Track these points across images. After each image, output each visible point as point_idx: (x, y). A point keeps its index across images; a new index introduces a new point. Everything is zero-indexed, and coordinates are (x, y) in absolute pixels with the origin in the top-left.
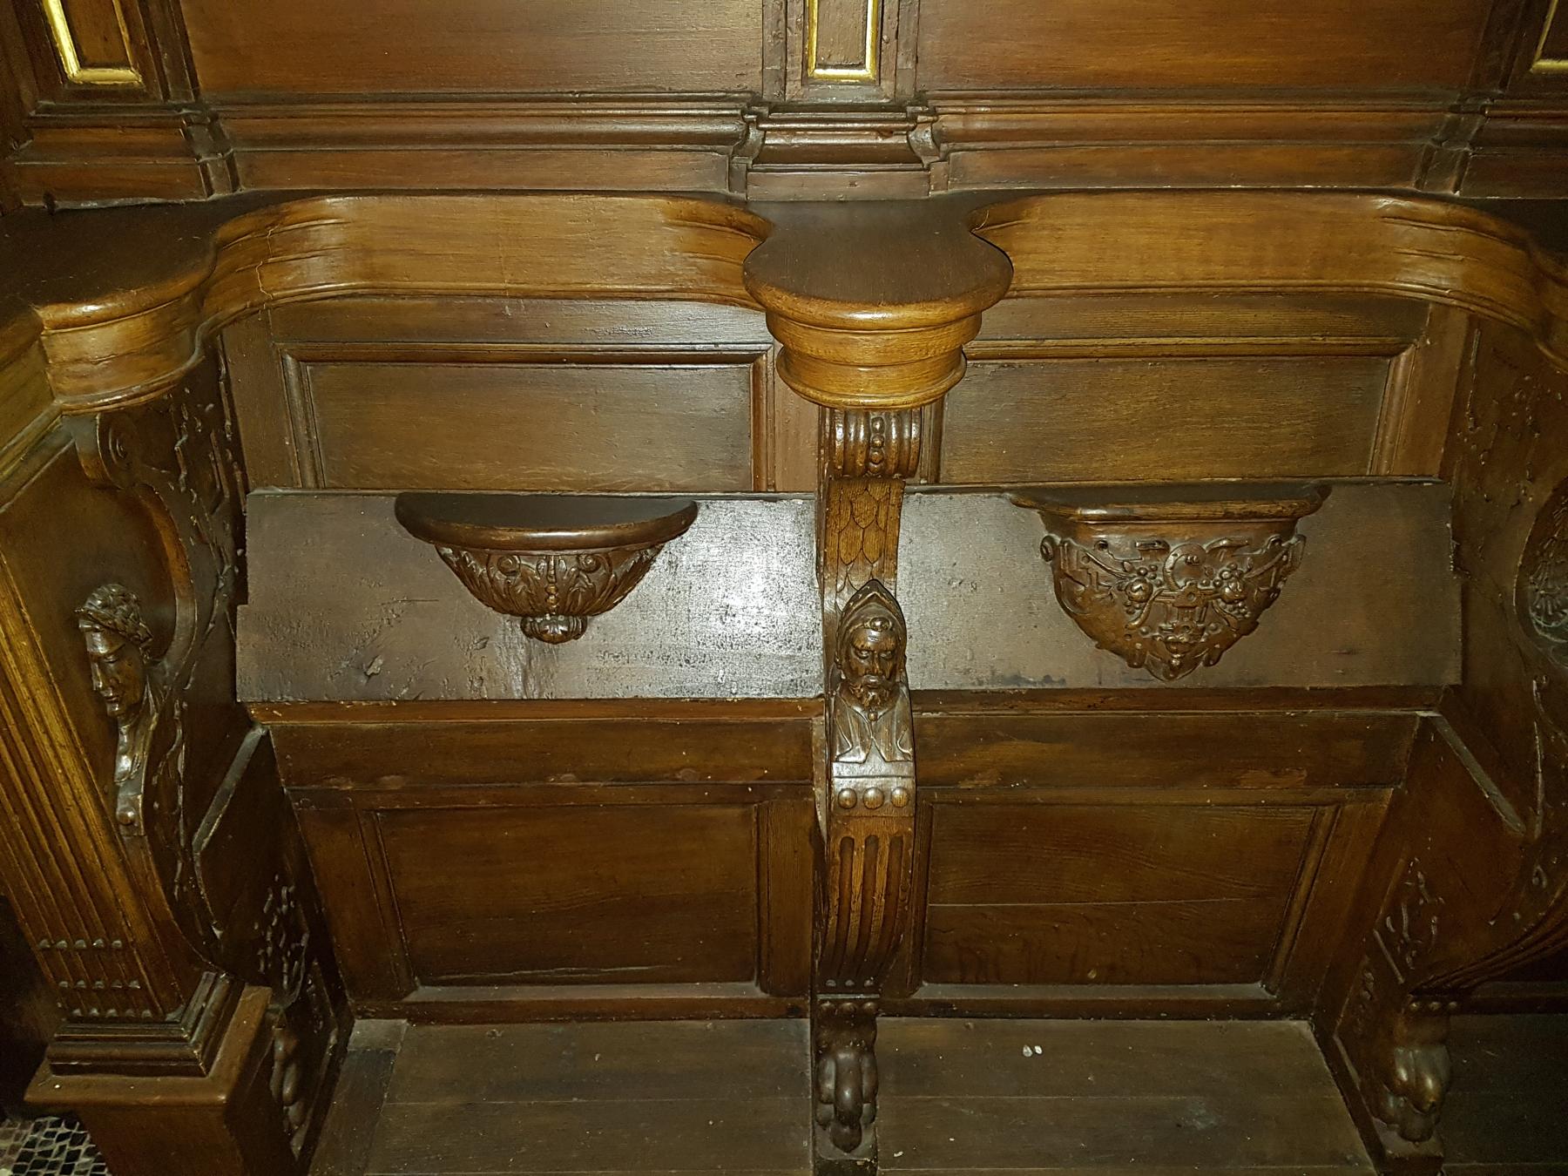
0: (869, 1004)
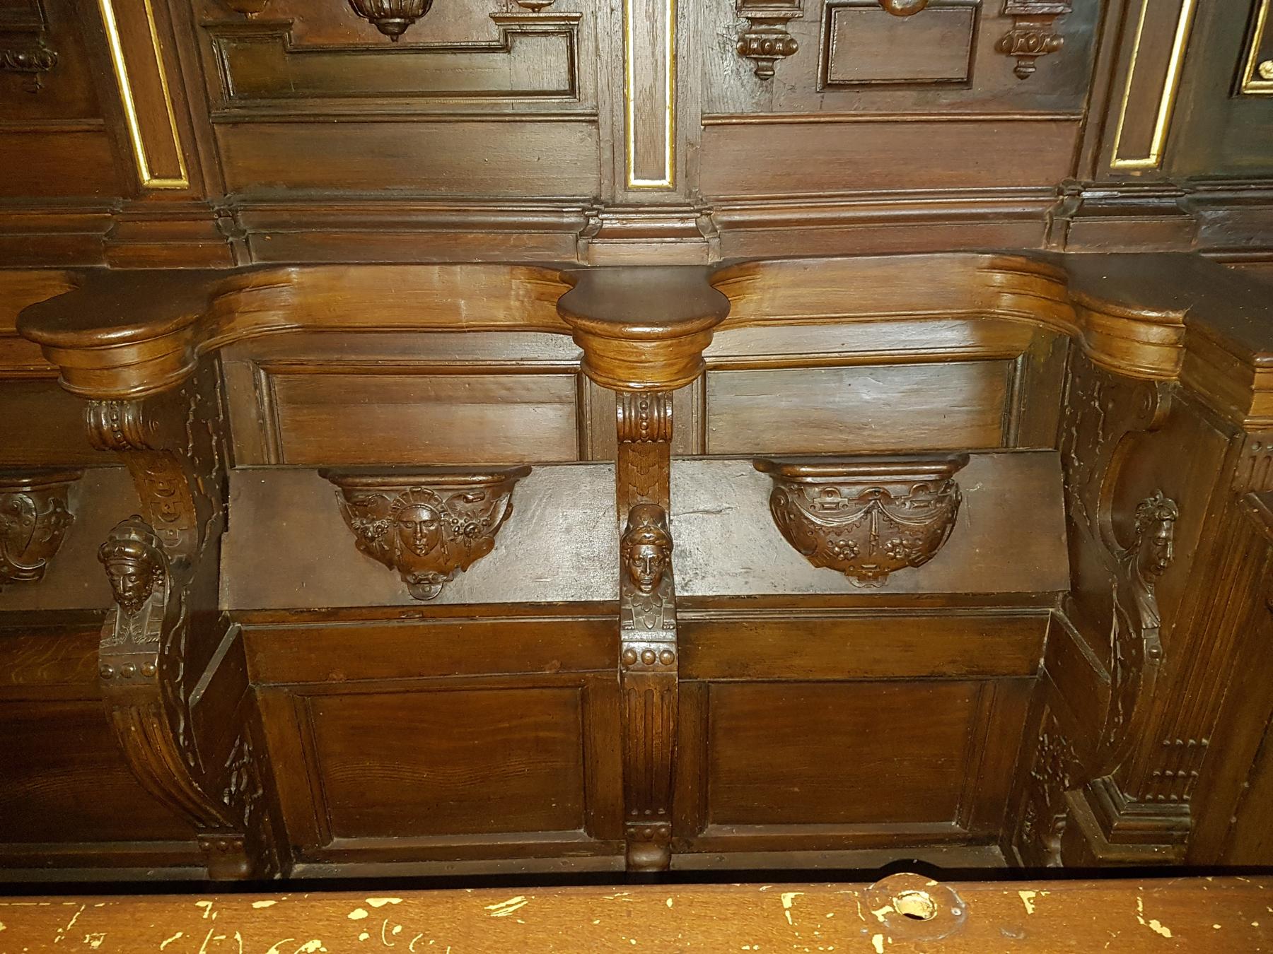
0: (663, 830)
